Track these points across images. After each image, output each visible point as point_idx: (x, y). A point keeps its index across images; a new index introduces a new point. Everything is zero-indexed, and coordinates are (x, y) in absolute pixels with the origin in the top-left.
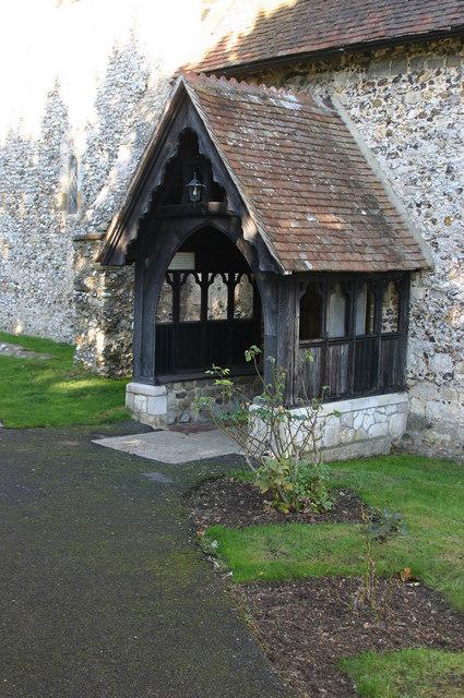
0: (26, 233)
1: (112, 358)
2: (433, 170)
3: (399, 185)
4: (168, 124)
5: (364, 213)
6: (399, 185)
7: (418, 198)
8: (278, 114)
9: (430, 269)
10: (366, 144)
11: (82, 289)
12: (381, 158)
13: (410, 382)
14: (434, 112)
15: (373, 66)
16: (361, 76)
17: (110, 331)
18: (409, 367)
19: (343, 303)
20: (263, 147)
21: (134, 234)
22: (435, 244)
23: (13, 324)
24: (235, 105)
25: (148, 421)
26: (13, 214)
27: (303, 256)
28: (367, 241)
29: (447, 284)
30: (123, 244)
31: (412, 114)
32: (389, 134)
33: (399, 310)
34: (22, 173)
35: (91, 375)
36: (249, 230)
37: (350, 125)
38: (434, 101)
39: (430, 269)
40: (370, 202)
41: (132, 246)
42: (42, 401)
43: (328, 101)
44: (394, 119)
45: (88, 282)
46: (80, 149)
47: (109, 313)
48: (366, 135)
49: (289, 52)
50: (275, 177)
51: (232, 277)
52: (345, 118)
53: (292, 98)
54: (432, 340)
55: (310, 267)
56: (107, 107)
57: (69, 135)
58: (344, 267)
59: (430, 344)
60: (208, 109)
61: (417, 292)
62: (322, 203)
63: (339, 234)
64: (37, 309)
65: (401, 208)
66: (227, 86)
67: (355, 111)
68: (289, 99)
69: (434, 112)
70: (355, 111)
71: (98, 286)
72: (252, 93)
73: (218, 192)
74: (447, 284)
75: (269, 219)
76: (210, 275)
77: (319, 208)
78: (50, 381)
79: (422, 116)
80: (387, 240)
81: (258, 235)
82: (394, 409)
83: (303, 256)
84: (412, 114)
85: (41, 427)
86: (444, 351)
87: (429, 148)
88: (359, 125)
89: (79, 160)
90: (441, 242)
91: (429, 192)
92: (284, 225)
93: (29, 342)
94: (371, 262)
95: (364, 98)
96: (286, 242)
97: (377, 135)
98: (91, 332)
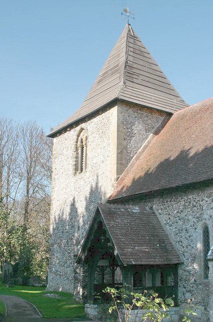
0: (64, 254)
1: (85, 297)
2: (182, 230)
3: (173, 235)
4: (95, 219)
5: (158, 245)
6: (173, 235)
7: (178, 240)
8: (132, 215)
9: (183, 263)
10: (163, 222)
11: (76, 273)
12: (167, 226)
13: (180, 303)
14: (182, 211)
15: (164, 196)
16: (161, 200)
17: (84, 288)
18: (179, 298)
19: (151, 276)
20: (123, 226)
21: (86, 253)
22: (184, 255)
23: (59, 289)
24: (115, 213)
25: (91, 317)
26: (60, 247)
27: (131, 260)
28: (158, 255)
29: (188, 268)
30: (83, 257)
31: (175, 212)
32: (169, 219)
33: (175, 277)
34: (63, 232)
35: (77, 303)
36: (116, 252)
37: (158, 216)
38: (181, 207)
39: (183, 263)
40: (161, 241)
41: (86, 258)
42: (58, 311)
43: (151, 208)
44: (170, 213)
45: (78, 271)
46: (81, 223)
47: (84, 281)
48: (163, 219)
49: (140, 192)
50: (126, 235)
51: (113, 268)
52: (157, 214)
53: (137, 208)
54: (185, 288)
55: (134, 263)
56: (89, 209)
57: (78, 219)
58: (147, 263)
59: (184, 289)
60: (105, 215)
61: (180, 272)
62: (142, 243)
63: (148, 253)
64: (66, 282)
65: (174, 243)
66: (112, 206)
67: (160, 211)
68: (136, 209)
69: (182, 211)
70: (160, 211)
71: (80, 271)
72: (122, 208)
73: (108, 240)
74: (188, 268)
75: (120, 248)
76: (115, 268)
77: (141, 245)
78: (62, 305)
79: (178, 212)
80: (166, 254)
81: (117, 254)
82: (174, 313)
83: (131, 260)
84: (175, 212)
85: (55, 318)
86: (189, 292)
87: (180, 223)
88: (161, 216)
89: (81, 228)
90: (185, 254)
91: (181, 237)
92: (129, 249)
93: (62, 294)
94: (158, 261)
95: (162, 207)
96: (126, 256)
97: (166, 219)
98: (79, 288)
